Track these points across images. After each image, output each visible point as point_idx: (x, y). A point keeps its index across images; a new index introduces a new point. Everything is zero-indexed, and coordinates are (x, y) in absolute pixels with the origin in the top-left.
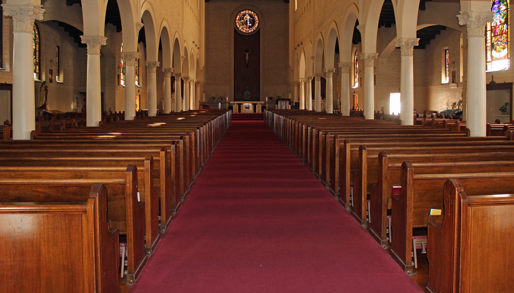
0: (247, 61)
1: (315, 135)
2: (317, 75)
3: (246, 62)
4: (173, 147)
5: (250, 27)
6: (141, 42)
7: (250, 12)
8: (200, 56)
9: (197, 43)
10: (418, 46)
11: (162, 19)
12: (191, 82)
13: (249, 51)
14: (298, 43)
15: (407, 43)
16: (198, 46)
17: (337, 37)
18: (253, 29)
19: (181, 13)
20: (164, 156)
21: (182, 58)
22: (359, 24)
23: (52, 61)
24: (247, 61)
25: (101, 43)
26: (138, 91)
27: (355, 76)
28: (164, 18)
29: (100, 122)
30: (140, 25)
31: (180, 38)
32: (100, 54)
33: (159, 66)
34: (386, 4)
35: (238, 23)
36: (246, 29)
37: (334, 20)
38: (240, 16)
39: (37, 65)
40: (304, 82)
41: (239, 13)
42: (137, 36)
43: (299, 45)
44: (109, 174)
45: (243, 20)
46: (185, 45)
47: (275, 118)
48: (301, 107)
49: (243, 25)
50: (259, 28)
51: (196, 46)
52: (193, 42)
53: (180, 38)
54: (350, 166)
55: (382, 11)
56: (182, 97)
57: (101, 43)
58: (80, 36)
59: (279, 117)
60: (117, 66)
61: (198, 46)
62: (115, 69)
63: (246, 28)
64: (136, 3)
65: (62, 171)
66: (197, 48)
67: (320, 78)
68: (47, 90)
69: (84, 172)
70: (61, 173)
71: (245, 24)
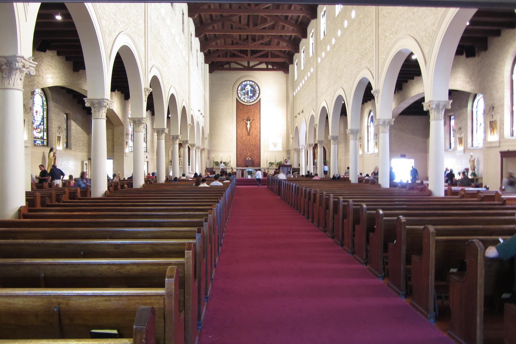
2: (321, 142)
4: (199, 237)
5: (251, 97)
6: (149, 110)
7: (251, 83)
8: (205, 125)
9: (202, 111)
10: (450, 109)
11: (170, 86)
12: (197, 149)
14: (299, 110)
15: (438, 106)
16: (203, 115)
22: (373, 89)
23: (60, 127)
28: (172, 86)
29: (106, 191)
31: (187, 105)
33: (167, 133)
35: (240, 93)
36: (247, 99)
37: (342, 86)
39: (45, 132)
41: (241, 84)
42: (145, 101)
44: (106, 300)
45: (245, 91)
46: (192, 113)
48: (302, 172)
49: (245, 95)
50: (259, 99)
51: (201, 114)
53: (187, 105)
56: (189, 165)
57: (107, 106)
58: (84, 99)
60: (125, 133)
61: (203, 115)
62: (123, 136)
63: (248, 98)
64: (144, 68)
65: (26, 296)
66: (202, 116)
68: (56, 157)
69: (62, 297)
70: (25, 299)
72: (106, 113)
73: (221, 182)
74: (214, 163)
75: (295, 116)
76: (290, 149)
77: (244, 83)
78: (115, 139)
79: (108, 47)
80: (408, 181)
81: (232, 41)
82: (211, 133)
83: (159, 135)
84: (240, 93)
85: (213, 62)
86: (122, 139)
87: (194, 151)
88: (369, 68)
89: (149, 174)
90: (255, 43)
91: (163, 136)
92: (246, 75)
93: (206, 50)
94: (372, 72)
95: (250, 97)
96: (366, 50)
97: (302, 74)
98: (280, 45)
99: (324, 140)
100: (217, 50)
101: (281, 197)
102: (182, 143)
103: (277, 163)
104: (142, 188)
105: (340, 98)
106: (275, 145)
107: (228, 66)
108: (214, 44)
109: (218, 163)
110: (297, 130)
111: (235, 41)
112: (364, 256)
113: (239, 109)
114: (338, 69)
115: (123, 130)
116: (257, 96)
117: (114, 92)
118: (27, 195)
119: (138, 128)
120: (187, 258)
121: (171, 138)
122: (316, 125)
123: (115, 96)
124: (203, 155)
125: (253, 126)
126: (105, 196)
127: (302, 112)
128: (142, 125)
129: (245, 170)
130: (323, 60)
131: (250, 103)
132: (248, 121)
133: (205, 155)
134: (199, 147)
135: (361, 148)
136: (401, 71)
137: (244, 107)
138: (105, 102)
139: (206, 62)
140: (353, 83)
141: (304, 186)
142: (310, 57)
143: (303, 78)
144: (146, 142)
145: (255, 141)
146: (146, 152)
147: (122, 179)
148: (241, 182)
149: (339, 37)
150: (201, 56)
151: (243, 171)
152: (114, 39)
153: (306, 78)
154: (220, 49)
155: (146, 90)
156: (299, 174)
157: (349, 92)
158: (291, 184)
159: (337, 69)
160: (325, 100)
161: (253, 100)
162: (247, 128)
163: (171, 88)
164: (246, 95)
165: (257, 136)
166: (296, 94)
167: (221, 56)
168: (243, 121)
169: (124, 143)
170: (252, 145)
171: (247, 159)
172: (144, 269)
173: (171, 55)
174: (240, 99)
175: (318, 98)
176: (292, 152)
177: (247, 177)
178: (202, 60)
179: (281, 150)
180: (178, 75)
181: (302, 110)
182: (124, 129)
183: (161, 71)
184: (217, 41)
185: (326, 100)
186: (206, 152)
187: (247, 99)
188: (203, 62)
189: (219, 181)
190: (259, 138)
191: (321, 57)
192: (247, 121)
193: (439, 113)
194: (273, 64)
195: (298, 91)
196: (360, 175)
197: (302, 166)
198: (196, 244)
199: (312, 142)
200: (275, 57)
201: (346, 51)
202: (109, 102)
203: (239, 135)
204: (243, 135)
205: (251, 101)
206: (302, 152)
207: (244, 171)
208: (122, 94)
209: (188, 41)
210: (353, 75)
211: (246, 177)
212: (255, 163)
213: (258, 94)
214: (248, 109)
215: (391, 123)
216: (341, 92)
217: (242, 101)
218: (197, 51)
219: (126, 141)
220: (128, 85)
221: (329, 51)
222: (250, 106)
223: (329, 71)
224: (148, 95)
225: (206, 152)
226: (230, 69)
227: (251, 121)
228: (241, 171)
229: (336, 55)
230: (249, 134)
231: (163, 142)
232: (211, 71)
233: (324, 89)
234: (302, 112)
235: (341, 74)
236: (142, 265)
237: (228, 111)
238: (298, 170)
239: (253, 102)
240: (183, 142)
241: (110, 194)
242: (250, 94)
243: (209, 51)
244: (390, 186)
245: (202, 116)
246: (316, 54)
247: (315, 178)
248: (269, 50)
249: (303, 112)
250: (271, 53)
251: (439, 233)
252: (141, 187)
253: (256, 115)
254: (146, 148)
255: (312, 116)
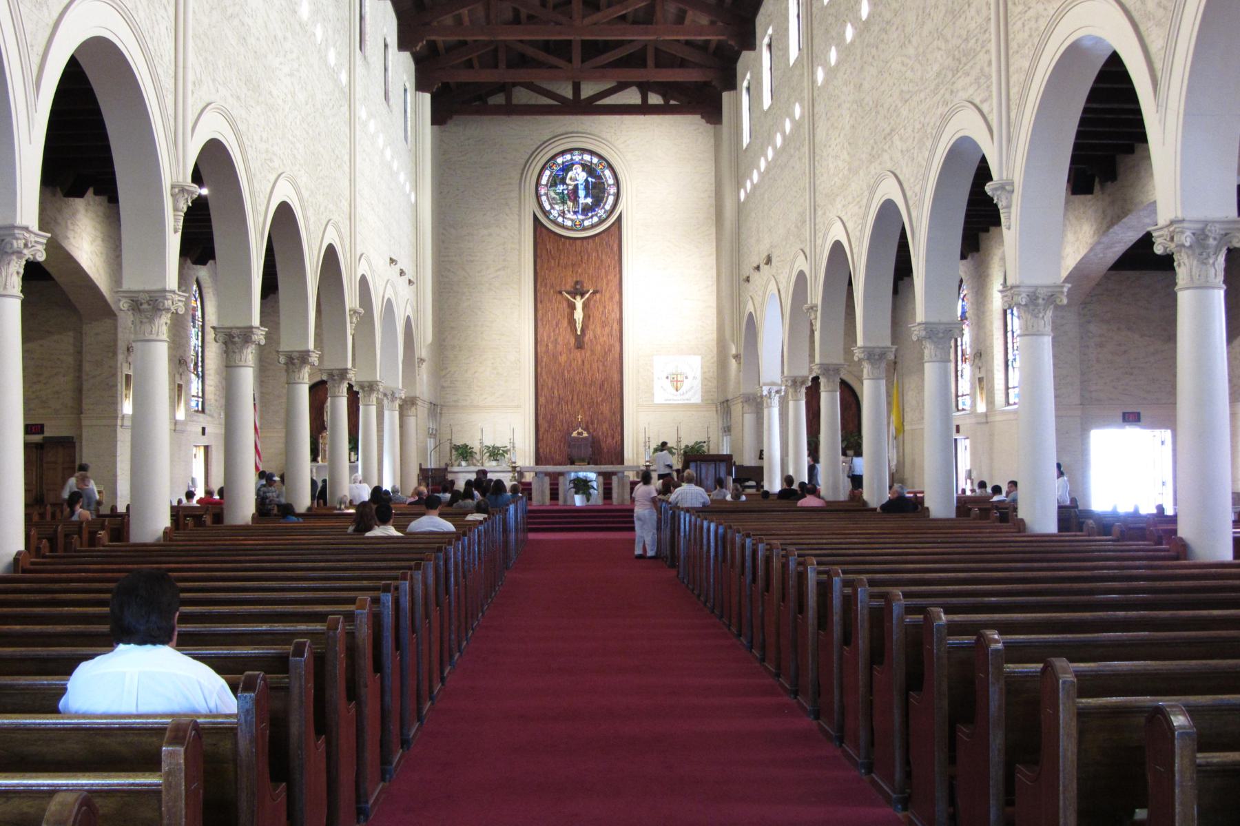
0: (579, 326)
1: (866, 611)
2: (827, 369)
3: (576, 330)
5: (587, 210)
7: (587, 157)
9: (405, 263)
13: (587, 292)
14: (756, 258)
15: (1201, 237)
16: (410, 274)
17: (903, 229)
18: (596, 215)
19: (346, 158)
20: (181, 769)
21: (351, 318)
23: (182, 361)
24: (579, 326)
25: (25, 251)
26: (200, 430)
27: (959, 374)
28: (282, 174)
29: (19, 553)
30: (187, 191)
31: (341, 239)
32: (21, 295)
33: (263, 342)
34: (1095, 106)
35: (546, 194)
36: (575, 217)
37: (893, 170)
38: (552, 173)
40: (778, 395)
41: (551, 163)
42: (176, 232)
43: (758, 268)
46: (362, 269)
47: (682, 526)
48: (771, 482)
49: (564, 202)
51: (402, 273)
52: (391, 259)
54: (1075, 786)
55: (1079, 135)
56: (354, 446)
57: (25, 251)
59: (702, 528)
61: (410, 274)
62: (115, 353)
63: (575, 213)
64: (171, 111)
66: (405, 279)
67: (839, 380)
71: (570, 199)
72: (21, 276)
73: (450, 521)
74: (453, 451)
75: (745, 277)
76: (730, 397)
77: (560, 160)
78: (87, 367)
79: (32, 46)
80: (1160, 509)
81: (516, 12)
82: (444, 340)
83: (234, 352)
84: (546, 194)
85: (446, 86)
86: (110, 367)
87: (373, 409)
88: (977, 101)
89: (209, 493)
90: (597, 17)
91: (249, 356)
92: (570, 129)
93: (420, 44)
94: (989, 118)
95: (583, 210)
96: (967, 40)
97: (765, 123)
98: (687, 21)
99: (842, 362)
100: (460, 41)
101: (678, 572)
102: (325, 378)
103: (683, 447)
104: (162, 542)
105: (888, 211)
106: (676, 382)
107: (504, 98)
108: (448, 20)
109: (466, 452)
110: (751, 328)
111: (524, 12)
112: (898, 775)
113: (544, 252)
114: (882, 106)
115: (116, 334)
116: (608, 207)
117: (81, 199)
119: (147, 327)
120: (169, 773)
121: (282, 360)
122: (813, 308)
123: (87, 210)
124: (412, 422)
125: (596, 314)
126: (16, 571)
127: (767, 264)
128: (163, 317)
129: (561, 474)
130: (831, 73)
131: (585, 229)
132: (578, 298)
133: (418, 420)
134: (393, 394)
135: (982, 389)
136: (1086, 110)
137: (561, 247)
138: (17, 236)
139: (420, 86)
140: (929, 162)
141: (739, 532)
142: (791, 64)
143: (770, 140)
144: (203, 377)
145: (601, 368)
146: (203, 411)
147: (105, 510)
148: (538, 520)
149: (826, 7)
150: (402, 66)
151: (554, 478)
152: (55, 15)
153: (779, 140)
154: (469, 38)
155: (177, 190)
156: (759, 486)
157: (917, 189)
158: (705, 523)
159: (876, 107)
160: (840, 218)
161: (595, 219)
162: (575, 320)
163: (278, 184)
164: (570, 204)
165: (610, 350)
166: (747, 196)
167: (476, 63)
168: (559, 297)
169: (119, 379)
170: (593, 383)
171: (575, 434)
172: (25, 810)
173: (281, 64)
174: (548, 217)
175: (820, 212)
176: (737, 409)
177: (569, 503)
178: (405, 78)
179: (696, 398)
180: (308, 133)
181: (766, 254)
182: (120, 330)
183: (238, 122)
184: (461, 11)
185: (844, 219)
186: (422, 410)
187: (575, 217)
188: (411, 85)
189: (442, 515)
190: (617, 356)
191: (825, 64)
192: (575, 298)
193: (1204, 262)
194: (665, 89)
195: (754, 187)
196: (978, 491)
197: (770, 458)
198: (239, 731)
199: (805, 371)
200: (672, 66)
201: (904, 43)
202: (33, 235)
203: (544, 349)
204: (559, 348)
205: (587, 223)
206: (769, 406)
207: (561, 479)
208: (111, 205)
209: (348, 14)
210: (929, 130)
211: (565, 501)
212: (605, 450)
213: (611, 200)
214: (578, 251)
215: (1058, 302)
216: (889, 190)
217: (555, 222)
218: (386, 46)
219: (126, 372)
220: (113, 173)
221: (852, 43)
222: (585, 243)
223: (851, 116)
224: (185, 210)
225: (422, 410)
226: (511, 110)
227: (587, 296)
228: (547, 480)
229: (873, 57)
230: (580, 344)
231: (247, 377)
232: (439, 118)
233: (836, 179)
234: (767, 264)
235: (890, 124)
236: (22, 795)
237: (504, 260)
238: (757, 473)
239: (593, 226)
240: (331, 375)
241: (33, 564)
242: (584, 200)
243: (432, 46)
244: (1060, 529)
245: (405, 279)
246: (810, 54)
247: (809, 501)
248: (650, 41)
249: (769, 260)
250: (657, 50)
251: (1088, 685)
252: (158, 540)
253: (607, 276)
254: (203, 397)
255: (801, 275)
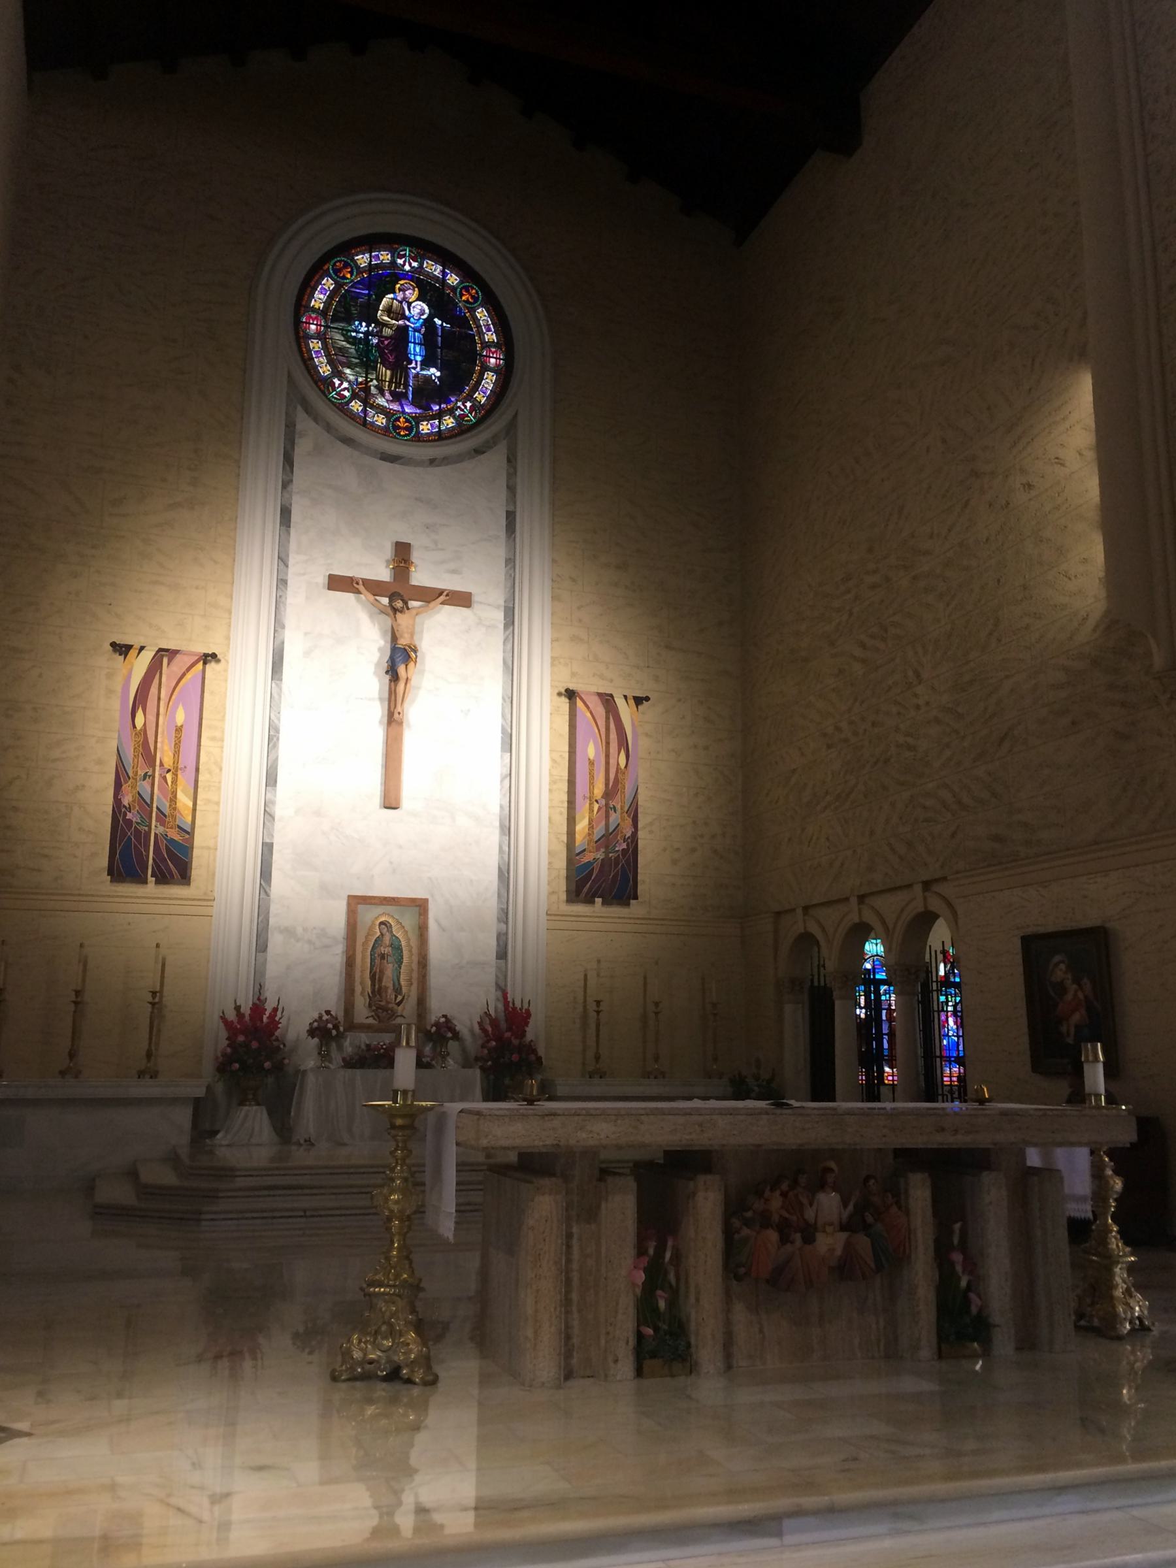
63: (397, 397)
118: (462, 1187)
